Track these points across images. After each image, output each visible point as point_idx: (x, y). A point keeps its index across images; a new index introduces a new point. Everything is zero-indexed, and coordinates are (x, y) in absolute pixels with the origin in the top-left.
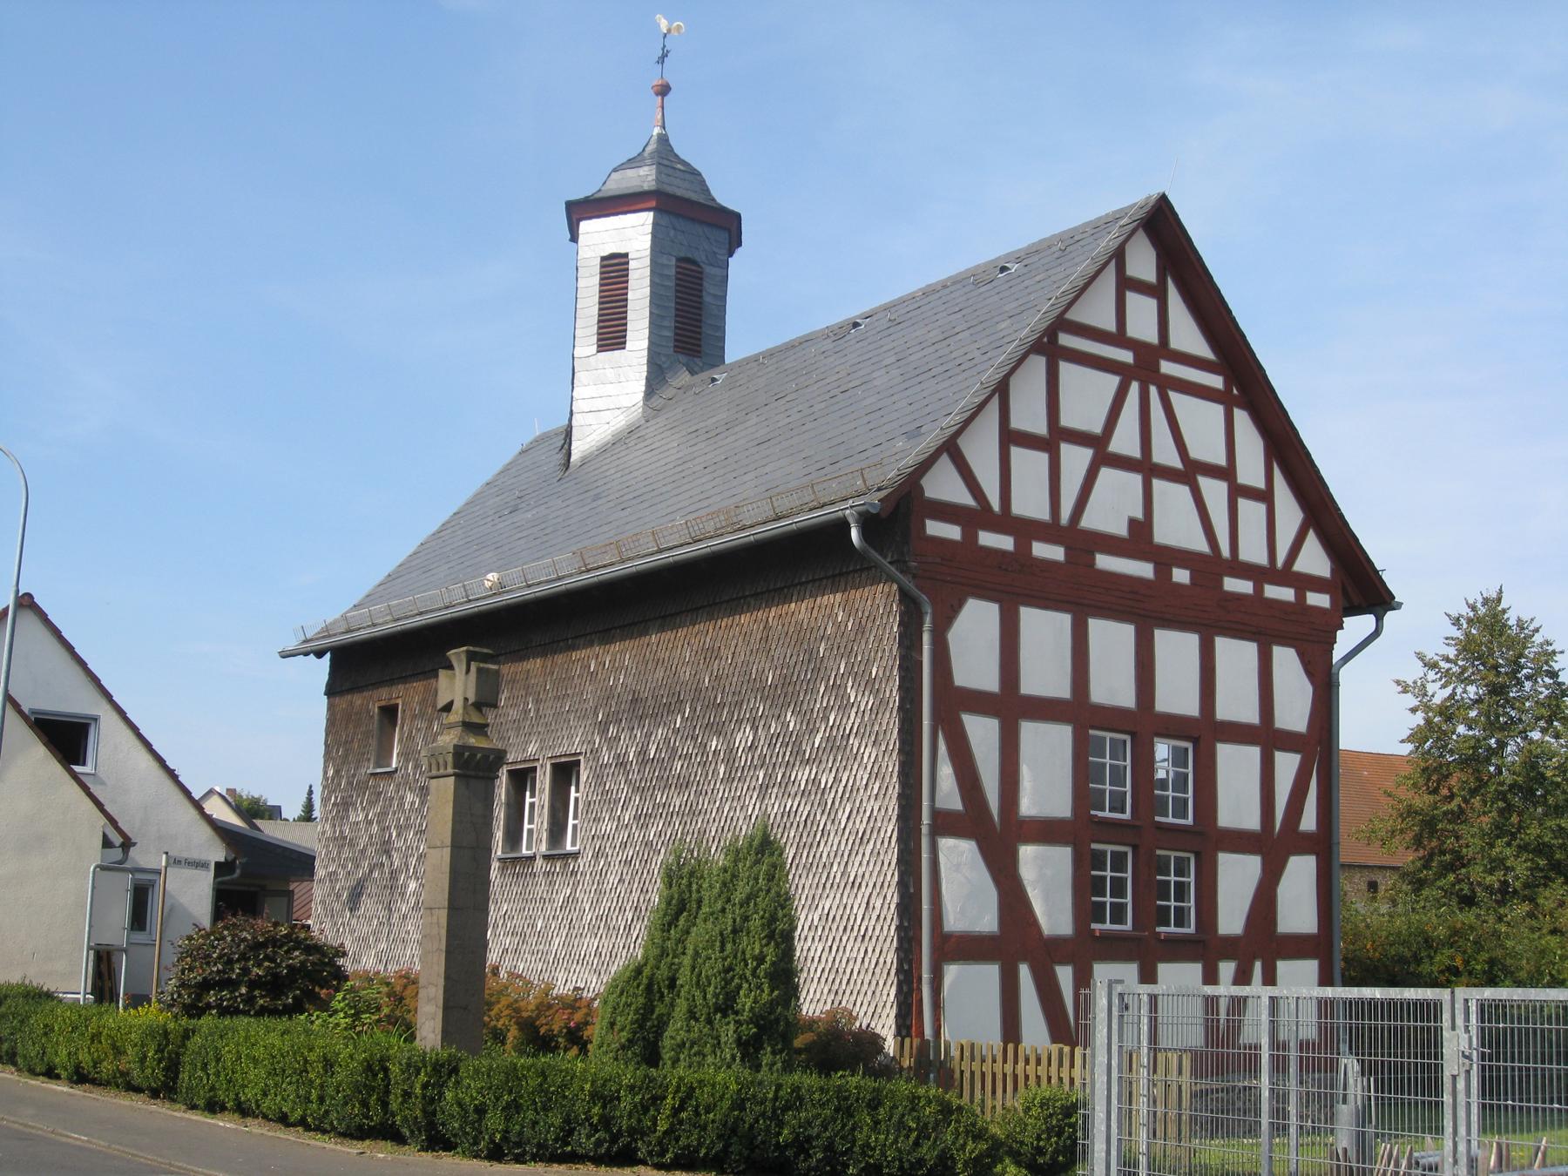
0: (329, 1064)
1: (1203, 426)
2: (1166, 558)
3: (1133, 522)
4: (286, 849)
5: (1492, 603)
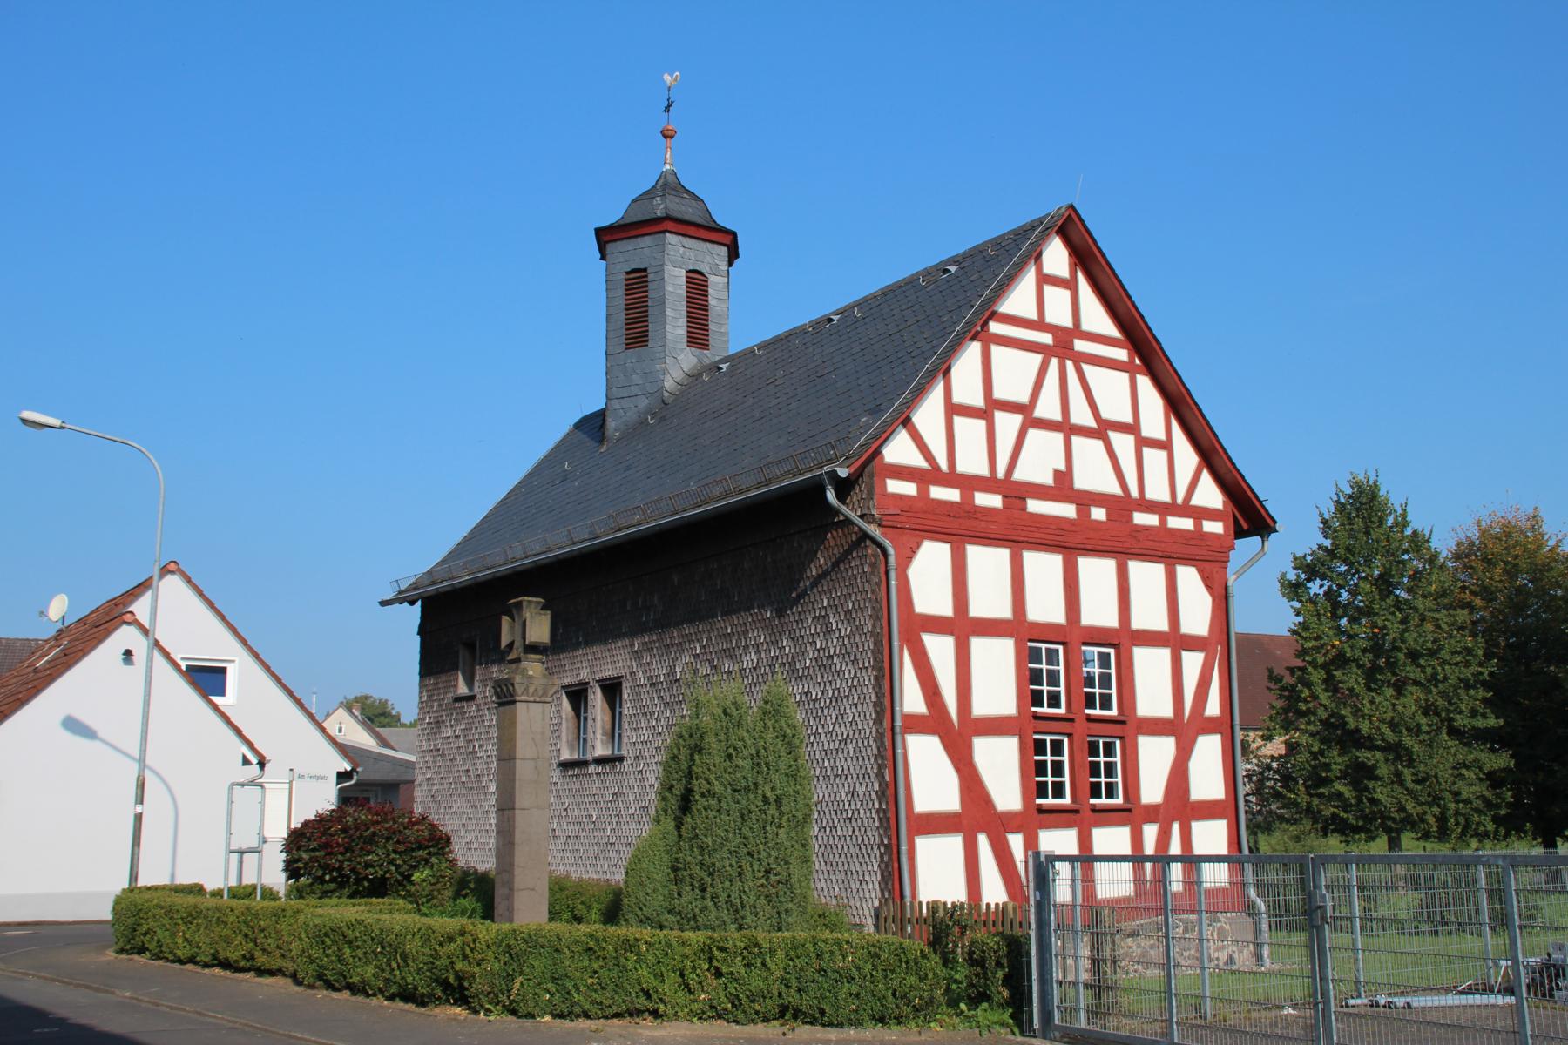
2: (1085, 500)
3: (1057, 473)
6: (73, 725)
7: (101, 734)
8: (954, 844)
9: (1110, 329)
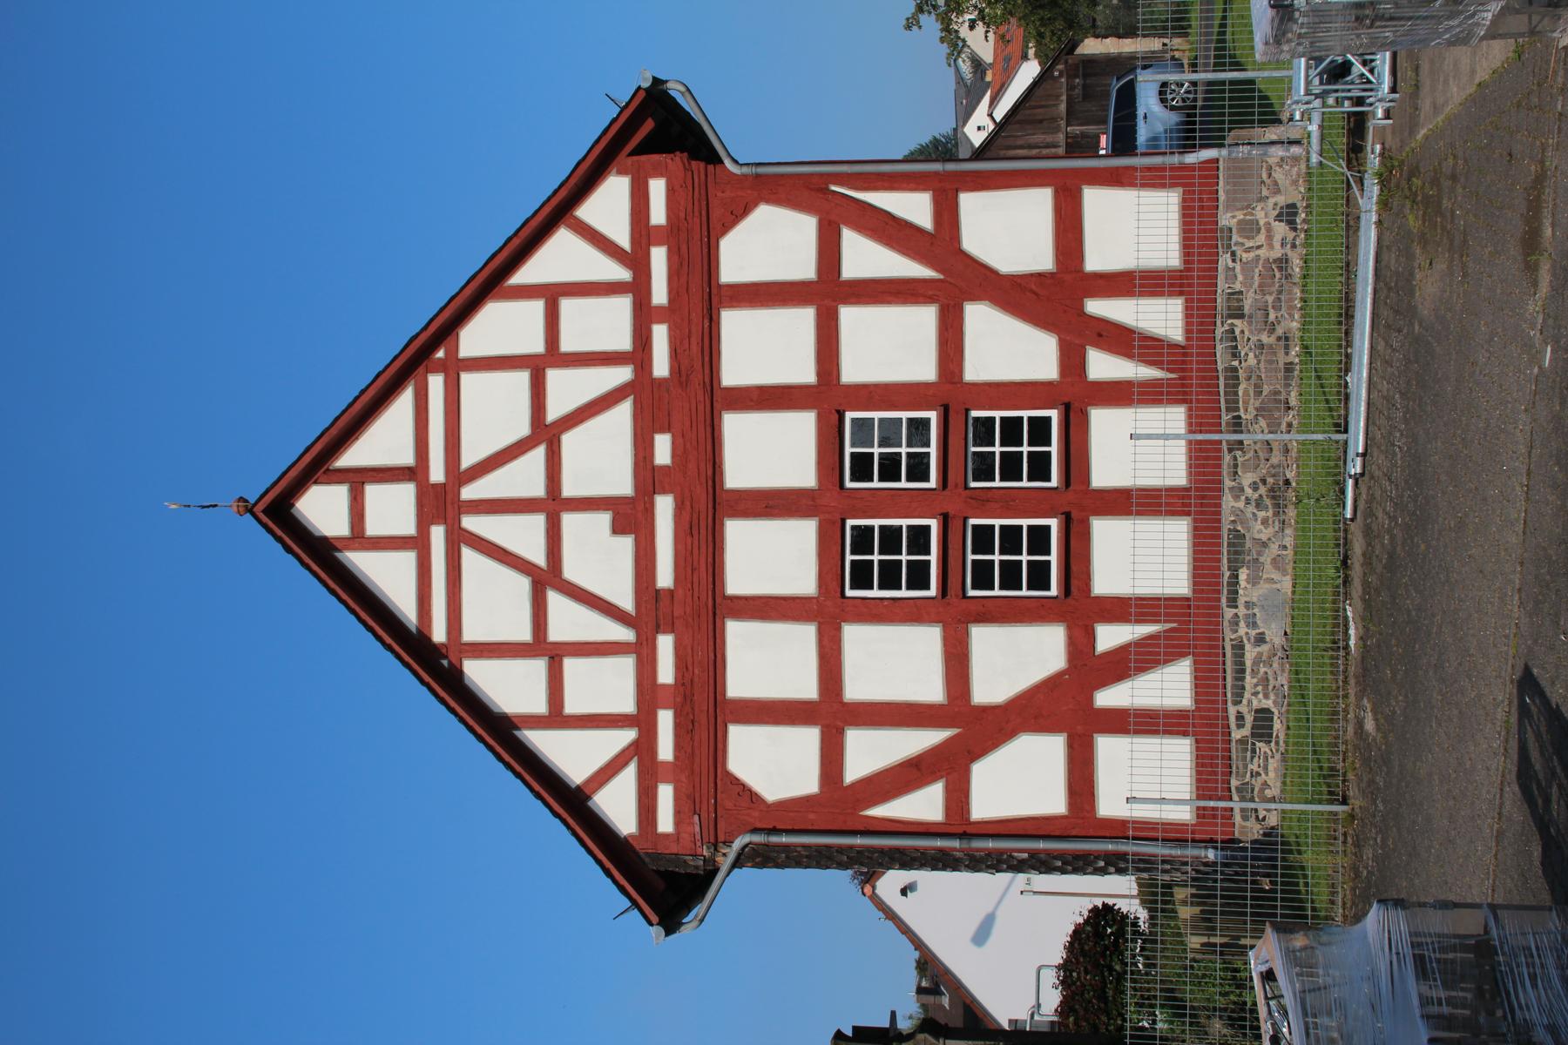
0: (1299, 852)
1: (493, 410)
2: (648, 478)
3: (618, 529)
4: (1093, 795)
5: (667, 934)
6: (982, 935)
7: (990, 910)
8: (1109, 749)
9: (402, 406)
